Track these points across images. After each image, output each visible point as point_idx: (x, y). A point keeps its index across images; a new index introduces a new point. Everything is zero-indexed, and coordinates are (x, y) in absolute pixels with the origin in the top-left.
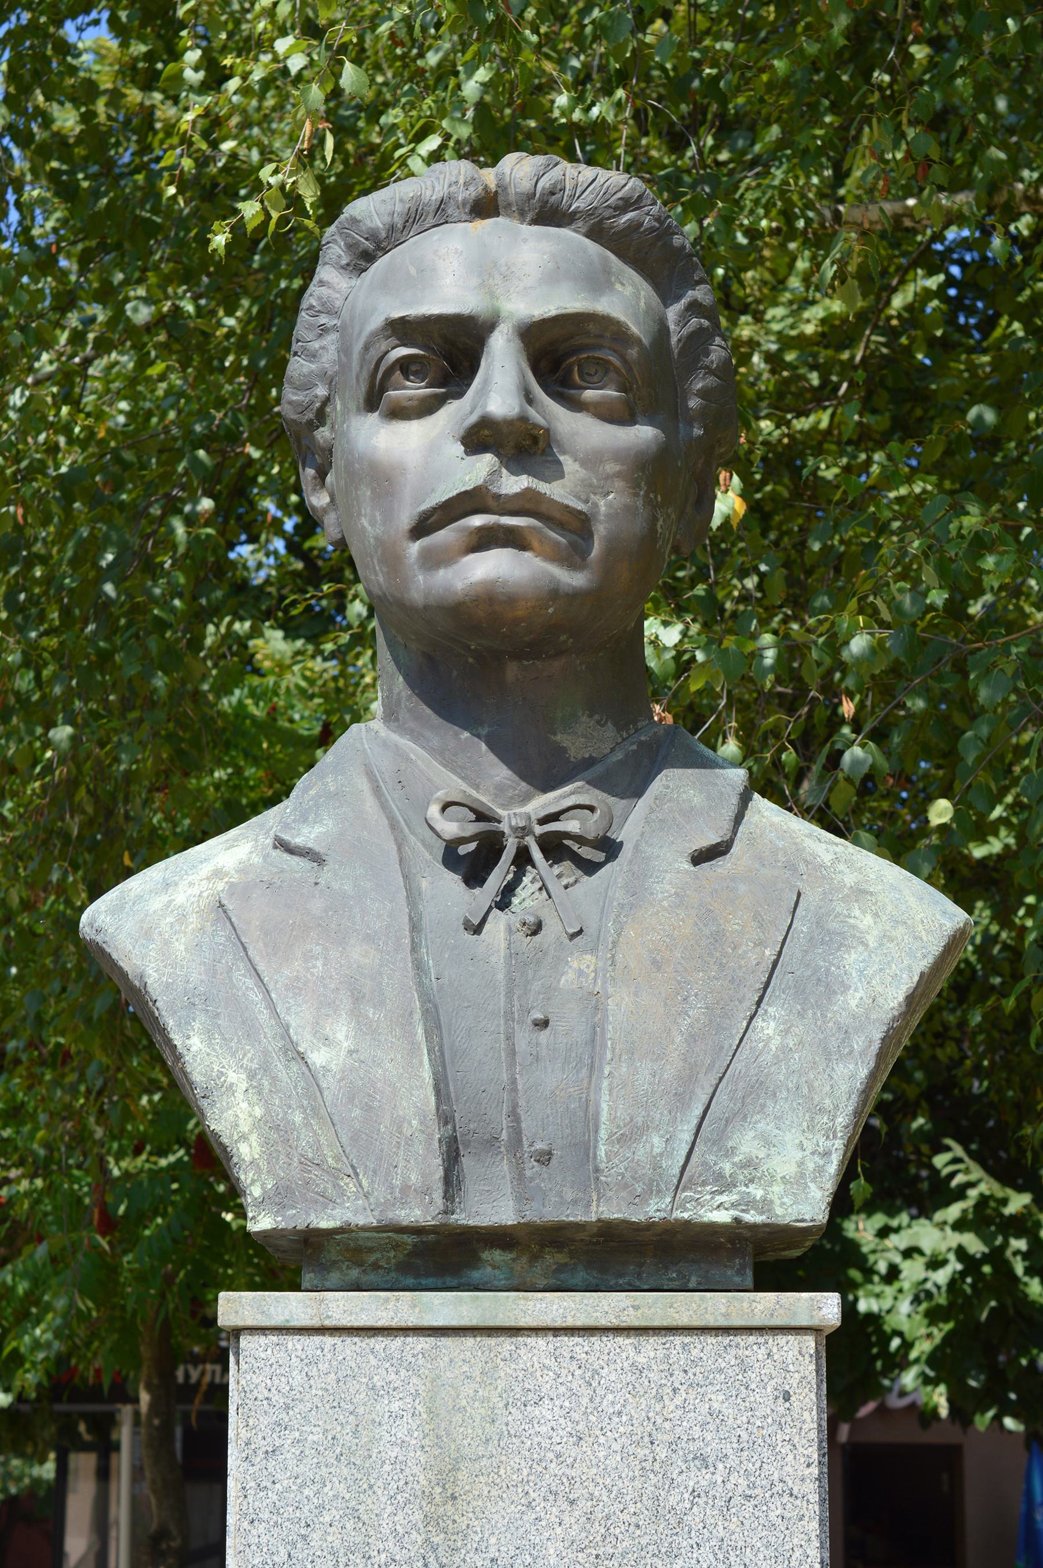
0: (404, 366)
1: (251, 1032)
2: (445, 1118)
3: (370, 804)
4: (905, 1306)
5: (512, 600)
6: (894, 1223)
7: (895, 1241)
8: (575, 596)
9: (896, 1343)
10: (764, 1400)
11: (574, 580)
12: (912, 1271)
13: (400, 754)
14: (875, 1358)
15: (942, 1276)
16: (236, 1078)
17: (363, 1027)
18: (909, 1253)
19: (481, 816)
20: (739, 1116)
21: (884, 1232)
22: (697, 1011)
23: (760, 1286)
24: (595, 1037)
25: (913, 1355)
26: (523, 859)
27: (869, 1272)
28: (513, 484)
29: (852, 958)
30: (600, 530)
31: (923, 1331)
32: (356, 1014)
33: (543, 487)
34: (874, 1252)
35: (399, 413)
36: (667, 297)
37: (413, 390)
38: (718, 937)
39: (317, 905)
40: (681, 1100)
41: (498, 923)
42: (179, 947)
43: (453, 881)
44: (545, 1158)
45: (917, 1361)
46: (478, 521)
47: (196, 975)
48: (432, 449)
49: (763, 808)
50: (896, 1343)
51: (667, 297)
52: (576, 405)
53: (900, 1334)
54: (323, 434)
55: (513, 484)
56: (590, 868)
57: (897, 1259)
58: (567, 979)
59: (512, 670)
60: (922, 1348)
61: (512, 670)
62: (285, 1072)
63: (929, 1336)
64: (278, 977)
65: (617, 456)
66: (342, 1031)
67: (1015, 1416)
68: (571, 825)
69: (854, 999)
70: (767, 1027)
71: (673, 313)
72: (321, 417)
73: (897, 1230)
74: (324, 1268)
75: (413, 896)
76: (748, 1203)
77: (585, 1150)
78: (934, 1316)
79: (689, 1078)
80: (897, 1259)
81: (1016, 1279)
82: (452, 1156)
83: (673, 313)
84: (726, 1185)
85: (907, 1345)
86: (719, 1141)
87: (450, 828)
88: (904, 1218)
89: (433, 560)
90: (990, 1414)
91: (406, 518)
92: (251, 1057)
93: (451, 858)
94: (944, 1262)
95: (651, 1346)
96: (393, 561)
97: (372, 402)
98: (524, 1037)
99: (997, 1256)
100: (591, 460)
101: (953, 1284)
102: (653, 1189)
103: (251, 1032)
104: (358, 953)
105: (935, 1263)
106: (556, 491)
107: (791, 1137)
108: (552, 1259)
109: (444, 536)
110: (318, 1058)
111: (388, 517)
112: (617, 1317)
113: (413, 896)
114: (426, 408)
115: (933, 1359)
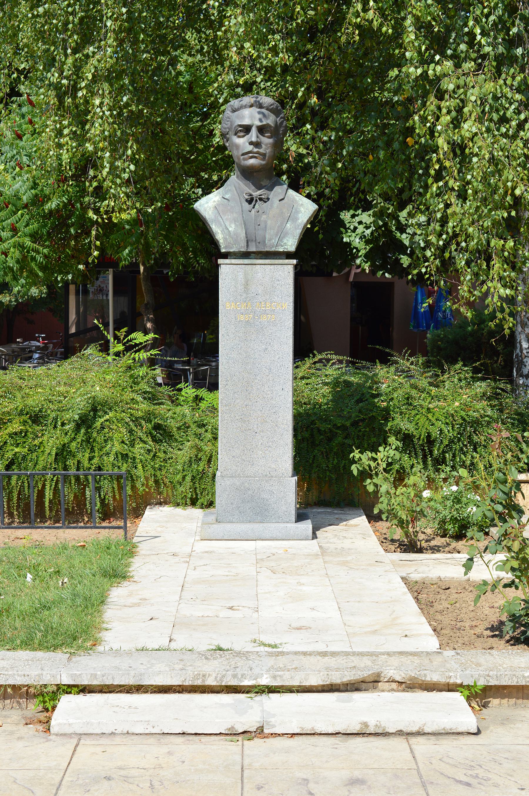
0: (240, 131)
1: (221, 225)
2: (247, 237)
3: (235, 192)
4: (357, 240)
5: (255, 166)
6: (357, 213)
7: (357, 219)
8: (264, 165)
9: (355, 250)
10: (286, 273)
11: (263, 162)
12: (361, 228)
13: (239, 184)
14: (349, 255)
15: (368, 232)
16: (219, 231)
17: (236, 225)
18: (360, 223)
19: (251, 195)
20: (284, 237)
21: (353, 216)
22: (279, 223)
23: (287, 259)
24: (266, 227)
25: (360, 254)
26: (256, 201)
27: (346, 229)
28: (256, 150)
29: (300, 215)
30: (267, 155)
31: (364, 247)
32: (235, 224)
33: (259, 150)
34: (349, 222)
35: (239, 137)
36: (277, 117)
37: (242, 134)
38: (282, 213)
39: (229, 208)
40: (277, 235)
41: (253, 211)
42: (210, 213)
43: (247, 204)
44: (259, 243)
45: (361, 256)
46: (251, 155)
47: (213, 217)
48: (244, 143)
49: (291, 192)
50: (355, 250)
51: (277, 117)
52: (264, 136)
53: (356, 248)
54: (228, 136)
55: (256, 150)
56: (265, 202)
57: (357, 225)
58: (262, 219)
59: (255, 174)
60: (362, 252)
61: (255, 174)
62: (226, 231)
63: (365, 248)
64: (224, 218)
65: (270, 144)
66: (233, 226)
67: (389, 273)
68: (263, 197)
69: (300, 221)
70: (288, 225)
71: (278, 119)
72: (228, 134)
73: (358, 215)
74: (231, 256)
75: (242, 206)
76: (285, 248)
77: (264, 242)
78: (367, 242)
79: (278, 232)
80: (357, 225)
81: (392, 232)
82: (247, 243)
83: (278, 119)
84: (282, 246)
85: (358, 251)
86: (281, 240)
87: (247, 197)
88: (360, 211)
89: (245, 159)
90: (381, 272)
91: (240, 153)
92: (221, 229)
93: (247, 200)
94: (370, 227)
95: (272, 266)
96: (239, 159)
97: (236, 134)
98: (257, 226)
99: (385, 225)
100: (266, 145)
101: (372, 233)
102: (273, 247)
103: (221, 225)
104: (235, 215)
105: (367, 228)
106: (261, 151)
107: (291, 240)
108: (260, 255)
109: (246, 156)
110: (230, 229)
111: (238, 152)
112: (274, 677)
113: (242, 206)
114: (243, 136)
115: (366, 256)
